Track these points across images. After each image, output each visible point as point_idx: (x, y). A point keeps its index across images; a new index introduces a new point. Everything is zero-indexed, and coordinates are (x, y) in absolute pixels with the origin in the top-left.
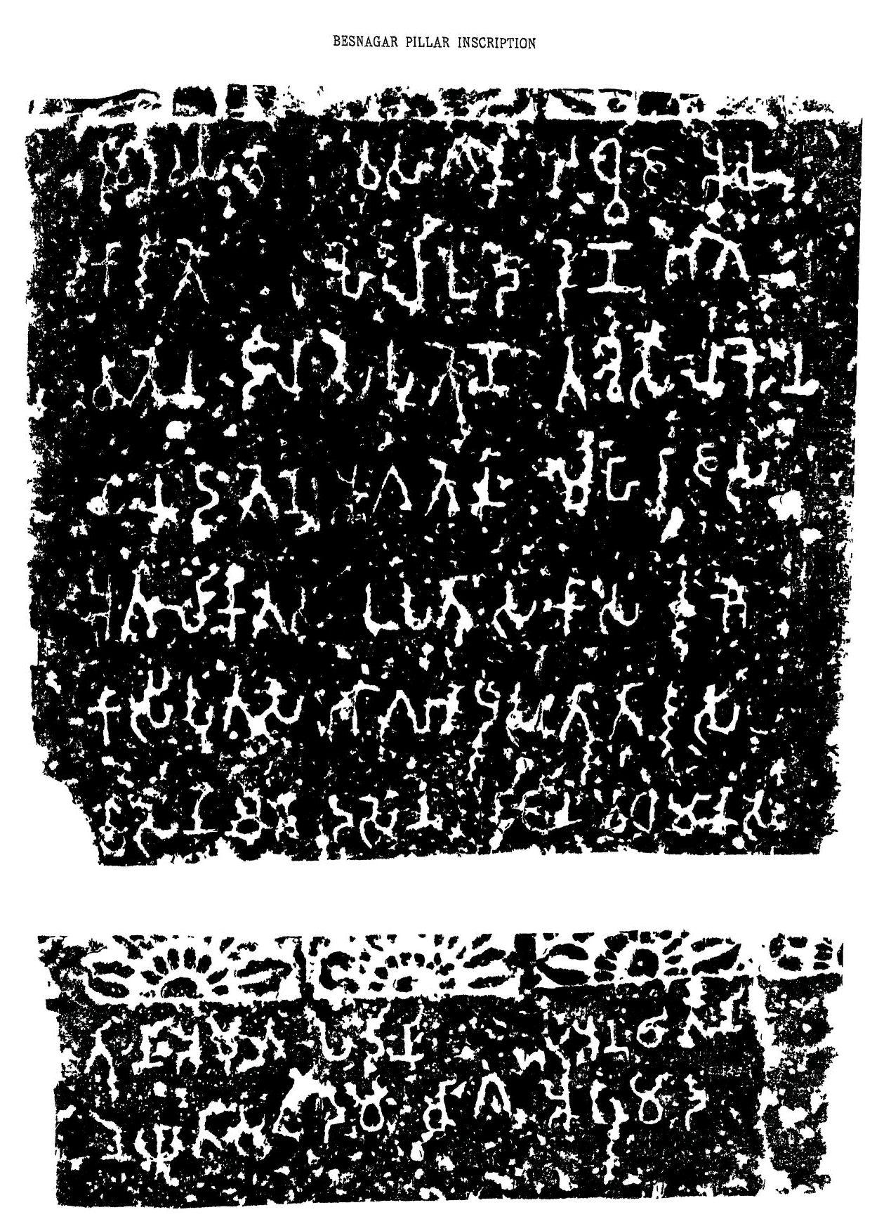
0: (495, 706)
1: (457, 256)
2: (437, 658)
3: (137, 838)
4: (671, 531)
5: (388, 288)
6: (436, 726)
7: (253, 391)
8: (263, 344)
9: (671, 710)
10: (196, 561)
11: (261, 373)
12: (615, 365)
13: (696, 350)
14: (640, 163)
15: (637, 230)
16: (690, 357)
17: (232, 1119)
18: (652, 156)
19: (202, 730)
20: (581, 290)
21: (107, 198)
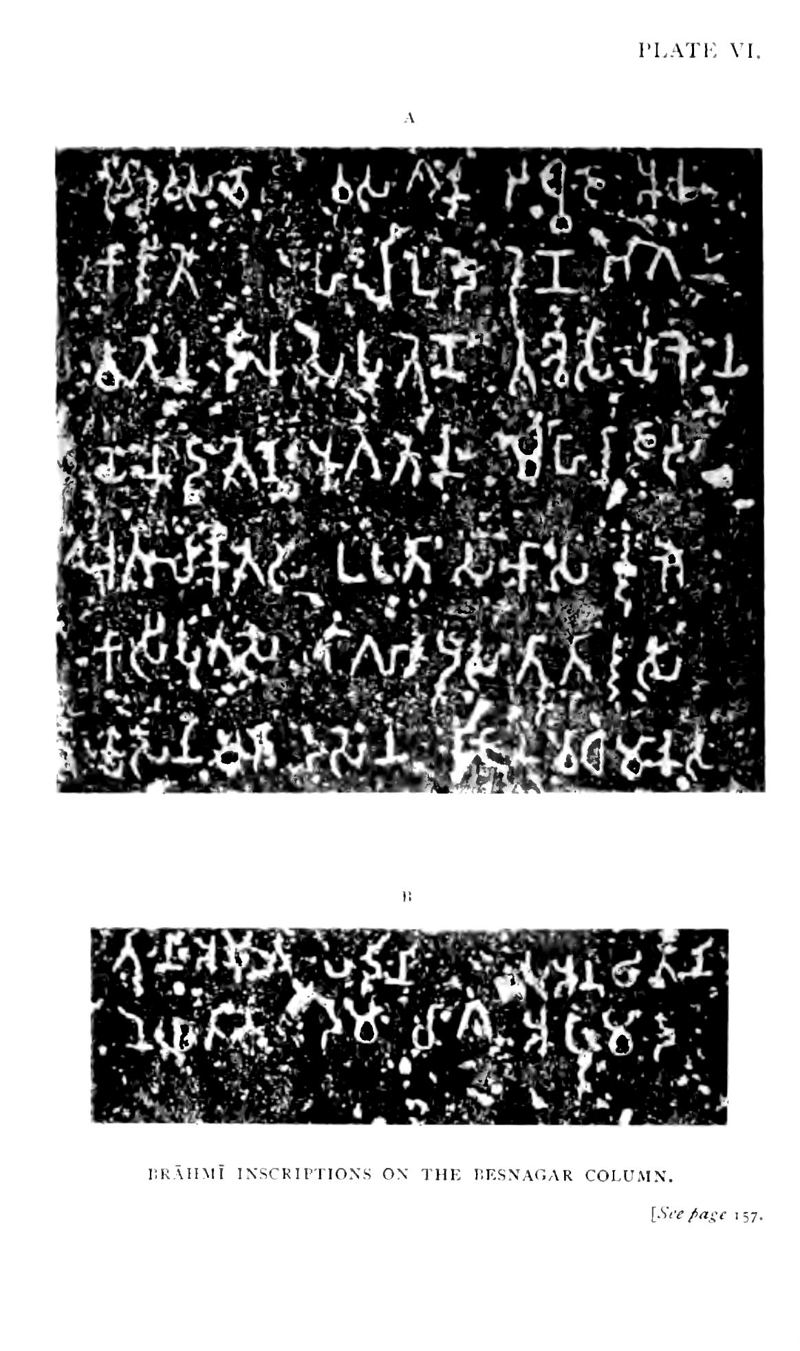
0: (457, 654)
1: (420, 259)
2: (402, 609)
3: (134, 762)
4: (615, 498)
5: (358, 285)
6: (399, 671)
7: (237, 375)
8: (245, 335)
9: (617, 659)
10: (186, 521)
11: (242, 360)
12: (561, 355)
13: (633, 342)
14: (582, 181)
15: (579, 240)
16: (628, 348)
17: (239, 1021)
18: (593, 173)
19: (193, 666)
20: (530, 291)
21: (112, 208)
